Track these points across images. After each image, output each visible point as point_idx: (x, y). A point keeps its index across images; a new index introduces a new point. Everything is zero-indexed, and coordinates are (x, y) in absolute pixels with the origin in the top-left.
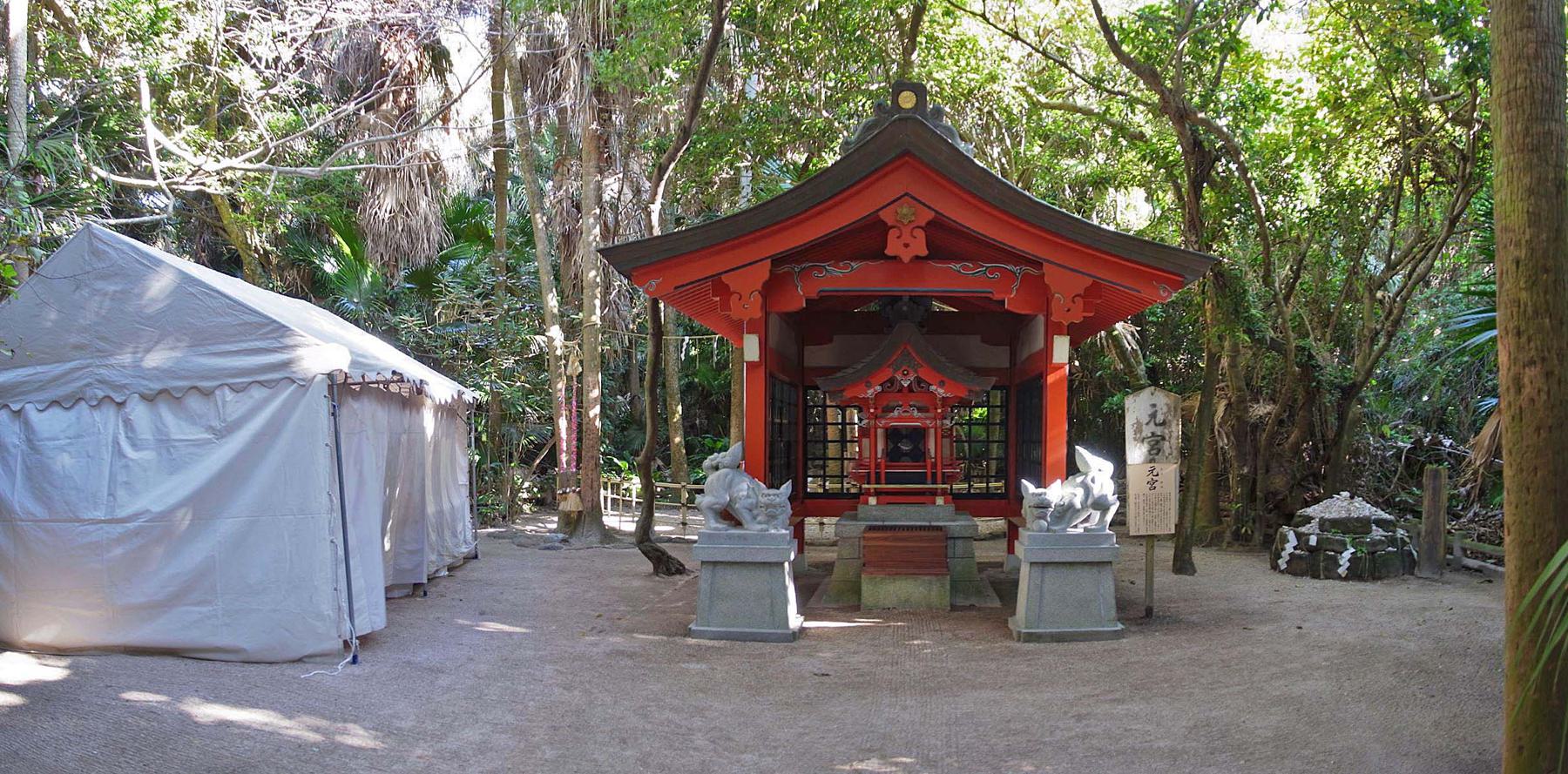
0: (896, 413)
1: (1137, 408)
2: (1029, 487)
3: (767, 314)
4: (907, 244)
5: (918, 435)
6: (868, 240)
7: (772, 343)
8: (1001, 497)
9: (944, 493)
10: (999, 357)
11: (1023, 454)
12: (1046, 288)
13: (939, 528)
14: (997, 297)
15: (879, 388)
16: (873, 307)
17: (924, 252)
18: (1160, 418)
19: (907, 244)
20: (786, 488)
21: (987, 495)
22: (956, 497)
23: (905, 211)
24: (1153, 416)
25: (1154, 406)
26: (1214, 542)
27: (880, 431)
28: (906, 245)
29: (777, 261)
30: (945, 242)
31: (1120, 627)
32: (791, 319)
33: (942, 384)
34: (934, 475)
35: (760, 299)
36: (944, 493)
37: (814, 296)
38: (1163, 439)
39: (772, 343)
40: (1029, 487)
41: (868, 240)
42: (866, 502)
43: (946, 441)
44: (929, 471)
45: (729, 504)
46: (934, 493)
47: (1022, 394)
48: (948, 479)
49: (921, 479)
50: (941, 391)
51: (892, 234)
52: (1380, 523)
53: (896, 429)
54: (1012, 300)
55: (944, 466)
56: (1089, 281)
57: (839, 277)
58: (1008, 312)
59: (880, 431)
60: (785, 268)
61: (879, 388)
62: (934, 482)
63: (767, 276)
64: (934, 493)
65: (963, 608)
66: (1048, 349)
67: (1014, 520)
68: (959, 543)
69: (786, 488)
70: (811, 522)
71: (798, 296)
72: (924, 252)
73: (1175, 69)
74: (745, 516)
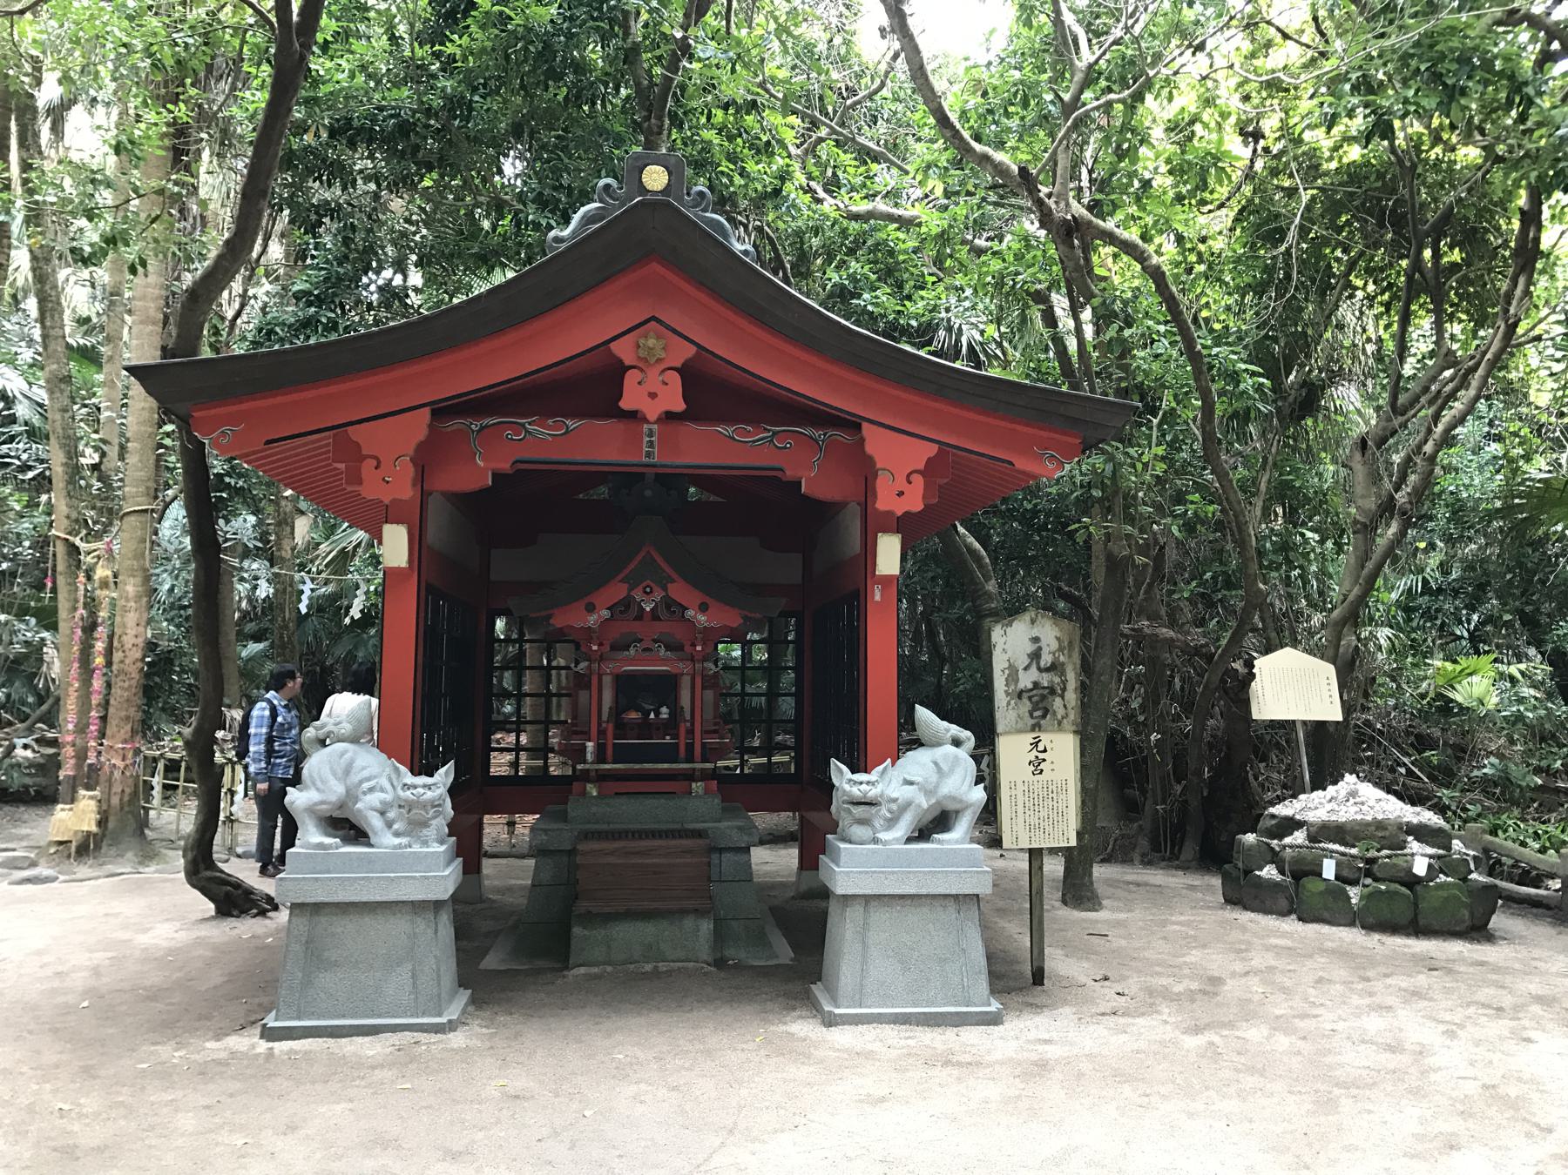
0: (632, 651)
1: (1018, 644)
2: (841, 775)
3: (424, 495)
4: (653, 392)
5: (664, 688)
6: (593, 388)
7: (433, 535)
8: (787, 778)
9: (705, 776)
10: (787, 569)
11: (837, 728)
12: (869, 461)
13: (699, 834)
14: (790, 474)
15: (606, 613)
16: (603, 491)
17: (679, 406)
18: (1046, 659)
19: (653, 392)
20: (445, 775)
21: (766, 776)
22: (725, 780)
23: (651, 342)
24: (1036, 656)
25: (1036, 640)
26: (1119, 854)
27: (607, 680)
28: (653, 396)
29: (442, 411)
30: (711, 392)
31: (994, 1006)
32: (469, 504)
33: (703, 608)
34: (690, 747)
35: (411, 470)
36: (705, 776)
37: (505, 466)
38: (1052, 691)
39: (433, 535)
40: (841, 775)
41: (593, 388)
42: (584, 793)
43: (709, 695)
44: (683, 741)
45: (342, 805)
46: (690, 777)
47: (824, 618)
48: (710, 754)
49: (670, 754)
50: (702, 618)
51: (631, 379)
52: (1422, 833)
53: (632, 676)
54: (816, 480)
55: (706, 732)
56: (933, 450)
57: (547, 439)
58: (805, 497)
59: (607, 680)
60: (456, 424)
61: (606, 613)
62: (690, 759)
63: (422, 434)
64: (690, 777)
65: (740, 968)
66: (869, 553)
67: (815, 817)
68: (726, 856)
69: (445, 775)
70: (494, 828)
71: (478, 470)
72: (679, 406)
73: (1081, 88)
74: (375, 822)
